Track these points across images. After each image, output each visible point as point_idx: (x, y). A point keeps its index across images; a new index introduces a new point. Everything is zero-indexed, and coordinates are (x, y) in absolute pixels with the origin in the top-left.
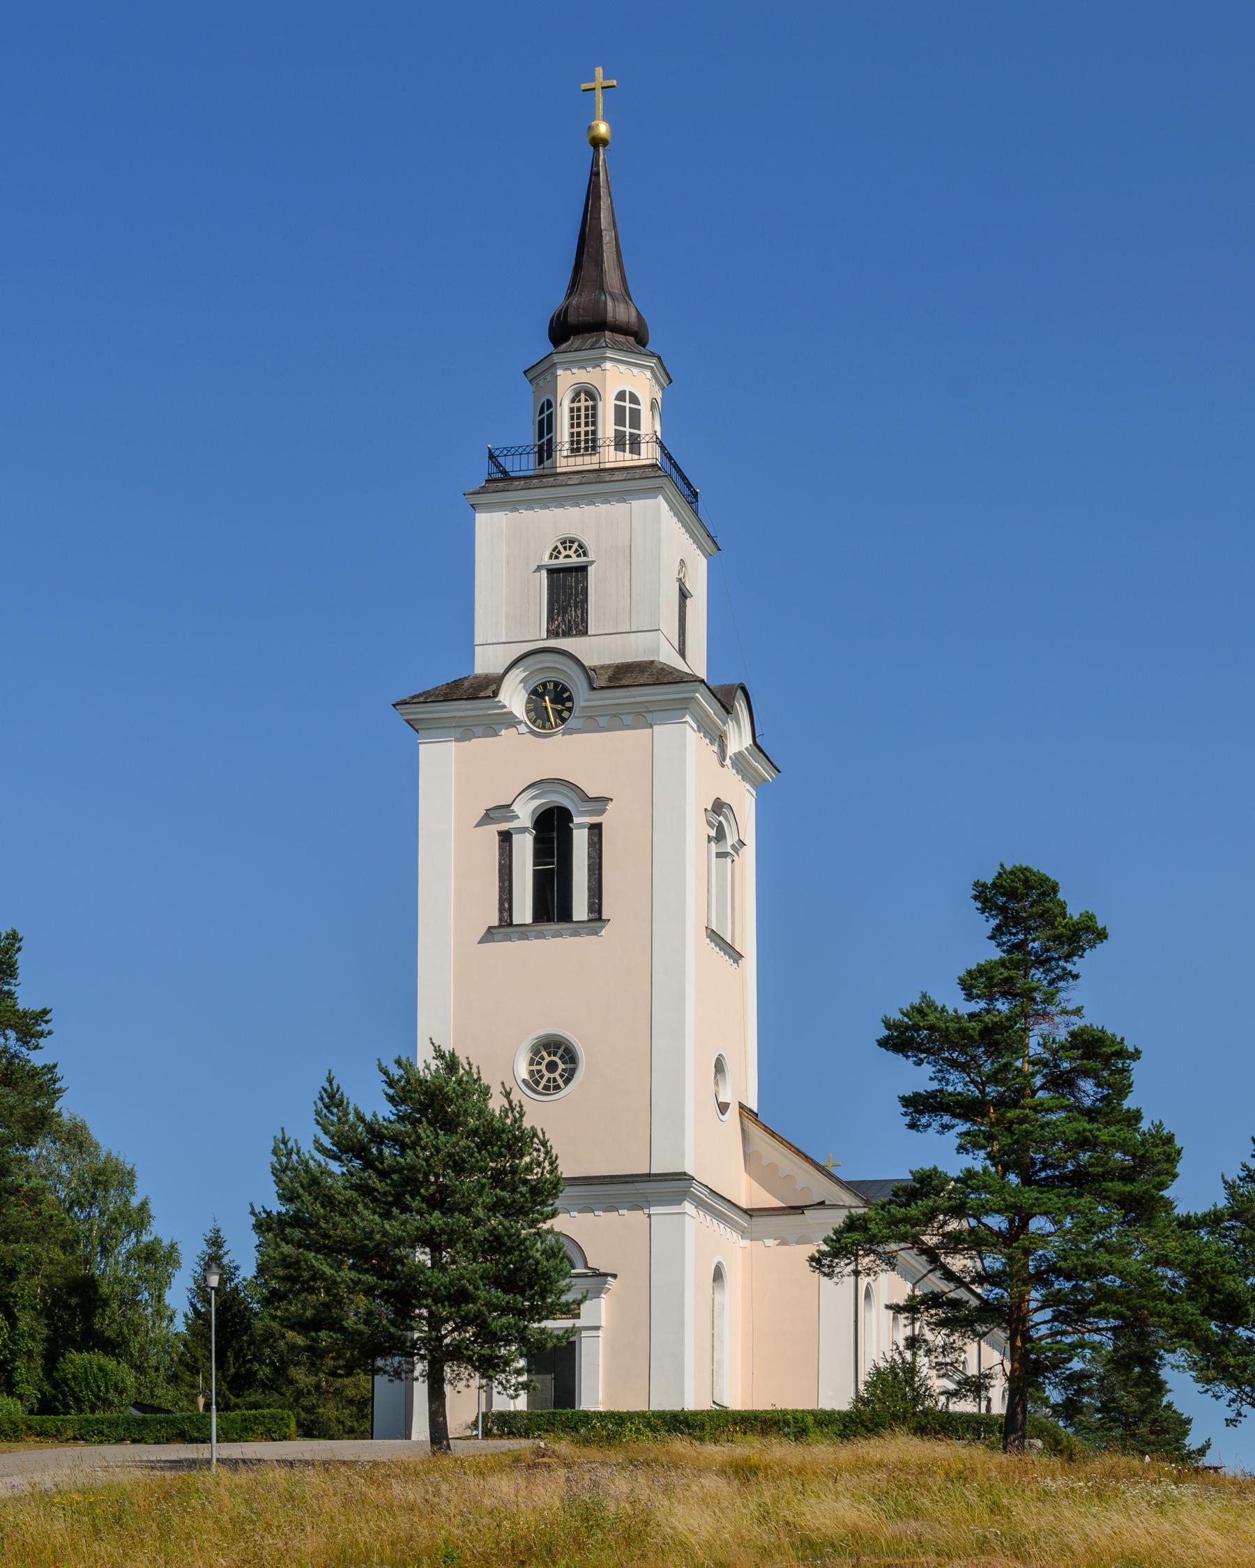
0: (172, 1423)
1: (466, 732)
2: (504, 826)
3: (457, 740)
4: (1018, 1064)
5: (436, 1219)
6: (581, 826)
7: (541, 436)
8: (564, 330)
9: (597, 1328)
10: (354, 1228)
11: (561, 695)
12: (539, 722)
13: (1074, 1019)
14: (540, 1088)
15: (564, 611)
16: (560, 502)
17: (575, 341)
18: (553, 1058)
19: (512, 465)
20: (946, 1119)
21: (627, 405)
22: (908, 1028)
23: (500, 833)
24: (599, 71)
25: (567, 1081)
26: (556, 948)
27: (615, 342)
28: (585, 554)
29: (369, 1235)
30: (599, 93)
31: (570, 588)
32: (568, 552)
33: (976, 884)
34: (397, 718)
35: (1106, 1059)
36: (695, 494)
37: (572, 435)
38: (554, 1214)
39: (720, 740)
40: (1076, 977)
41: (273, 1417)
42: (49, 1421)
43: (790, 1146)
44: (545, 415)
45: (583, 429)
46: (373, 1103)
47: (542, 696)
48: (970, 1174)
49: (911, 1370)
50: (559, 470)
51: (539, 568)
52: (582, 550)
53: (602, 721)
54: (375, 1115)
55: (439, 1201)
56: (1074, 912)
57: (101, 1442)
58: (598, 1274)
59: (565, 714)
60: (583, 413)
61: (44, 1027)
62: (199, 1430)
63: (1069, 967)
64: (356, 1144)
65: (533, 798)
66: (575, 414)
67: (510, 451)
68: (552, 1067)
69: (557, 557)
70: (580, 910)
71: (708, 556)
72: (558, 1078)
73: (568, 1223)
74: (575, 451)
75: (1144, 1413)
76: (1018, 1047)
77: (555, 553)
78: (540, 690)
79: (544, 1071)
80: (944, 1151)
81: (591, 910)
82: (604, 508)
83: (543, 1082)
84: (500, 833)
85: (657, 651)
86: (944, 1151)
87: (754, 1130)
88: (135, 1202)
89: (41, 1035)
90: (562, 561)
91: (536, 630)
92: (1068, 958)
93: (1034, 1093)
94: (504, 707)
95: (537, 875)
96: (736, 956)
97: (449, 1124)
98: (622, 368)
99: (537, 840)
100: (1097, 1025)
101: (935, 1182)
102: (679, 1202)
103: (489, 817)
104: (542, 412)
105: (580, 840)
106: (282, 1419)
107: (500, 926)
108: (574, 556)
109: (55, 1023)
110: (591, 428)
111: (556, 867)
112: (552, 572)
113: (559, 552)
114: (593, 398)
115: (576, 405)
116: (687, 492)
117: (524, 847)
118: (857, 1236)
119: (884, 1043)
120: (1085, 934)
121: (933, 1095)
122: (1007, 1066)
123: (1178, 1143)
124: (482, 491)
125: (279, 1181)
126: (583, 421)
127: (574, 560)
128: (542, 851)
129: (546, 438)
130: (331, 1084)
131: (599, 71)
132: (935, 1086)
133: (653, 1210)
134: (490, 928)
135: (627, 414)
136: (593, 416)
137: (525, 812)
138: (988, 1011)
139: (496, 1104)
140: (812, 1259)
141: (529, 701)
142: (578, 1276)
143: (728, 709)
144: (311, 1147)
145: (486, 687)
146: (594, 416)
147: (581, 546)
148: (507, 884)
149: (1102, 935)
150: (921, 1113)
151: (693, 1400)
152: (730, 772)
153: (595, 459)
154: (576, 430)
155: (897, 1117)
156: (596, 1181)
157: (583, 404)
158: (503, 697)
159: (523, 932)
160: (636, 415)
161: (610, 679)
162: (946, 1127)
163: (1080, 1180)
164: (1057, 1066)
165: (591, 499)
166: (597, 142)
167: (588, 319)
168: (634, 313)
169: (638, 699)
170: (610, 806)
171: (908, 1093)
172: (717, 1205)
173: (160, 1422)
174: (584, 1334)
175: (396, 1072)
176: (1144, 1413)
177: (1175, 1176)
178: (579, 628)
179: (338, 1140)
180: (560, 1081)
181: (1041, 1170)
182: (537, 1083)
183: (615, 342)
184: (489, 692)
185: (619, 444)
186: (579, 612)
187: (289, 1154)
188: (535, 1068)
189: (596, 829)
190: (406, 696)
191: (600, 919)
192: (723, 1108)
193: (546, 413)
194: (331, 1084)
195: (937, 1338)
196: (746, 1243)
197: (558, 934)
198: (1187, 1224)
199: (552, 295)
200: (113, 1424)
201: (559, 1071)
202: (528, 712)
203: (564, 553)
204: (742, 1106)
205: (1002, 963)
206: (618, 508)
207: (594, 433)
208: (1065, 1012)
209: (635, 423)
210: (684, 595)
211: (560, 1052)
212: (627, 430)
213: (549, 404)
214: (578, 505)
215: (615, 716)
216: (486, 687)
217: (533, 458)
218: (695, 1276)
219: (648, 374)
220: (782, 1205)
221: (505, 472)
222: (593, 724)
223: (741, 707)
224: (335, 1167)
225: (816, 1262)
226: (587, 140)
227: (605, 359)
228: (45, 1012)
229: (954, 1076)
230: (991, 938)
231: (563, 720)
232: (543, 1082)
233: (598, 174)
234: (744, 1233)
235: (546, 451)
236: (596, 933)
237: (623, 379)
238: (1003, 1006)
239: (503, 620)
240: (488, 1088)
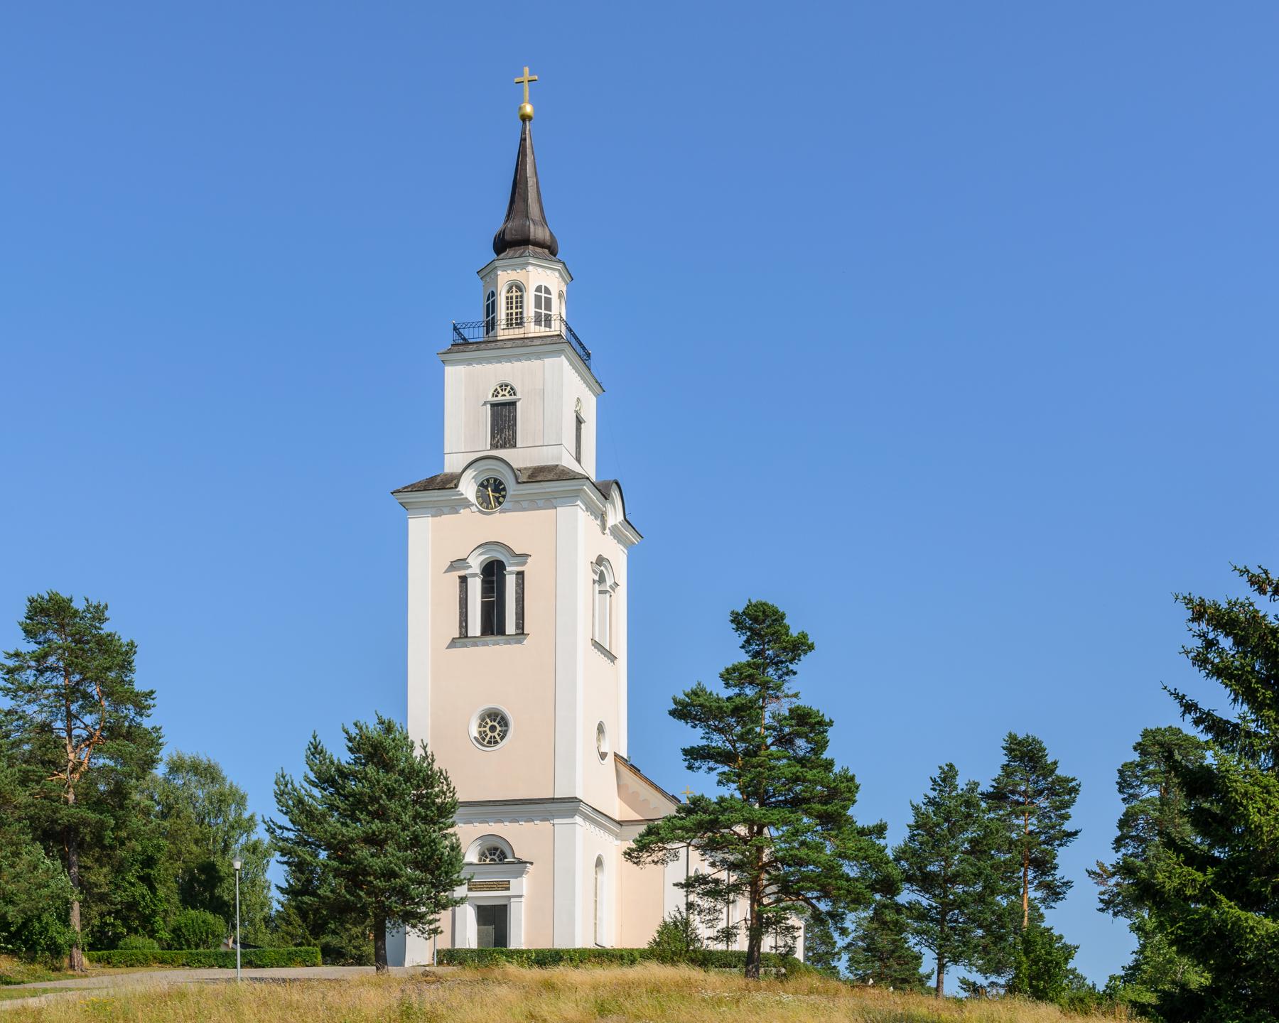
1: (438, 511)
2: (462, 573)
4: (758, 730)
5: (377, 825)
6: (511, 573)
8: (503, 245)
10: (326, 831)
11: (498, 487)
13: (794, 700)
15: (501, 431)
16: (499, 359)
17: (509, 252)
20: (712, 764)
21: (543, 295)
22: (688, 705)
23: (460, 577)
24: (526, 70)
25: (502, 738)
26: (495, 651)
27: (535, 252)
29: (334, 836)
30: (526, 84)
33: (732, 613)
34: (394, 501)
35: (812, 727)
36: (589, 355)
38: (452, 825)
39: (602, 517)
40: (795, 673)
41: (307, 952)
42: (168, 954)
45: (514, 311)
46: (341, 755)
47: (486, 487)
48: (722, 800)
49: (687, 923)
51: (485, 403)
53: (525, 504)
55: (381, 815)
56: (794, 633)
61: (150, 702)
63: (791, 667)
64: (330, 778)
67: (468, 325)
68: (493, 729)
70: (510, 628)
71: (597, 395)
74: (509, 324)
75: (893, 952)
76: (757, 720)
80: (708, 785)
81: (517, 627)
82: (526, 363)
84: (460, 577)
85: (560, 458)
86: (708, 785)
87: (625, 771)
88: (246, 815)
89: (149, 707)
90: (500, 399)
91: (483, 443)
92: (791, 661)
93: (768, 747)
96: (613, 658)
97: (387, 766)
98: (540, 270)
99: (484, 582)
100: (808, 704)
101: (703, 804)
102: (572, 816)
105: (511, 581)
109: (159, 701)
111: (495, 598)
112: (494, 405)
116: (582, 353)
117: (475, 586)
118: (652, 838)
119: (673, 713)
120: (799, 647)
121: (702, 748)
122: (750, 731)
123: (857, 781)
124: (449, 352)
125: (279, 801)
127: (508, 398)
131: (526, 70)
132: (704, 742)
133: (556, 821)
135: (543, 301)
137: (476, 564)
138: (739, 695)
139: (418, 753)
140: (625, 853)
141: (478, 491)
142: (509, 863)
143: (606, 496)
144: (302, 779)
145: (450, 482)
149: (811, 647)
150: (696, 759)
151: (582, 941)
152: (609, 538)
153: (522, 331)
155: (680, 762)
157: (514, 294)
158: (461, 488)
159: (475, 642)
160: (548, 301)
161: (529, 477)
162: (711, 769)
163: (796, 803)
164: (781, 730)
165: (518, 358)
166: (525, 118)
168: (548, 233)
170: (529, 560)
171: (687, 747)
172: (598, 817)
175: (354, 731)
176: (893, 952)
177: (855, 802)
178: (510, 442)
179: (319, 775)
181: (773, 796)
183: (535, 252)
185: (538, 321)
187: (286, 786)
189: (520, 575)
190: (399, 488)
192: (603, 756)
195: (705, 903)
196: (618, 842)
197: (497, 643)
198: (862, 832)
199: (495, 222)
200: (207, 956)
204: (616, 755)
205: (749, 665)
206: (535, 364)
208: (787, 696)
209: (548, 307)
210: (579, 421)
212: (543, 311)
213: (493, 294)
216: (450, 482)
217: (482, 331)
218: (583, 864)
219: (557, 274)
221: (464, 339)
222: (519, 506)
223: (615, 495)
224: (316, 792)
225: (628, 854)
227: (529, 264)
228: (152, 692)
229: (716, 736)
230: (743, 647)
231: (500, 503)
233: (525, 140)
234: (617, 836)
235: (491, 325)
237: (540, 277)
238: (750, 691)
239: (462, 438)
240: (413, 743)
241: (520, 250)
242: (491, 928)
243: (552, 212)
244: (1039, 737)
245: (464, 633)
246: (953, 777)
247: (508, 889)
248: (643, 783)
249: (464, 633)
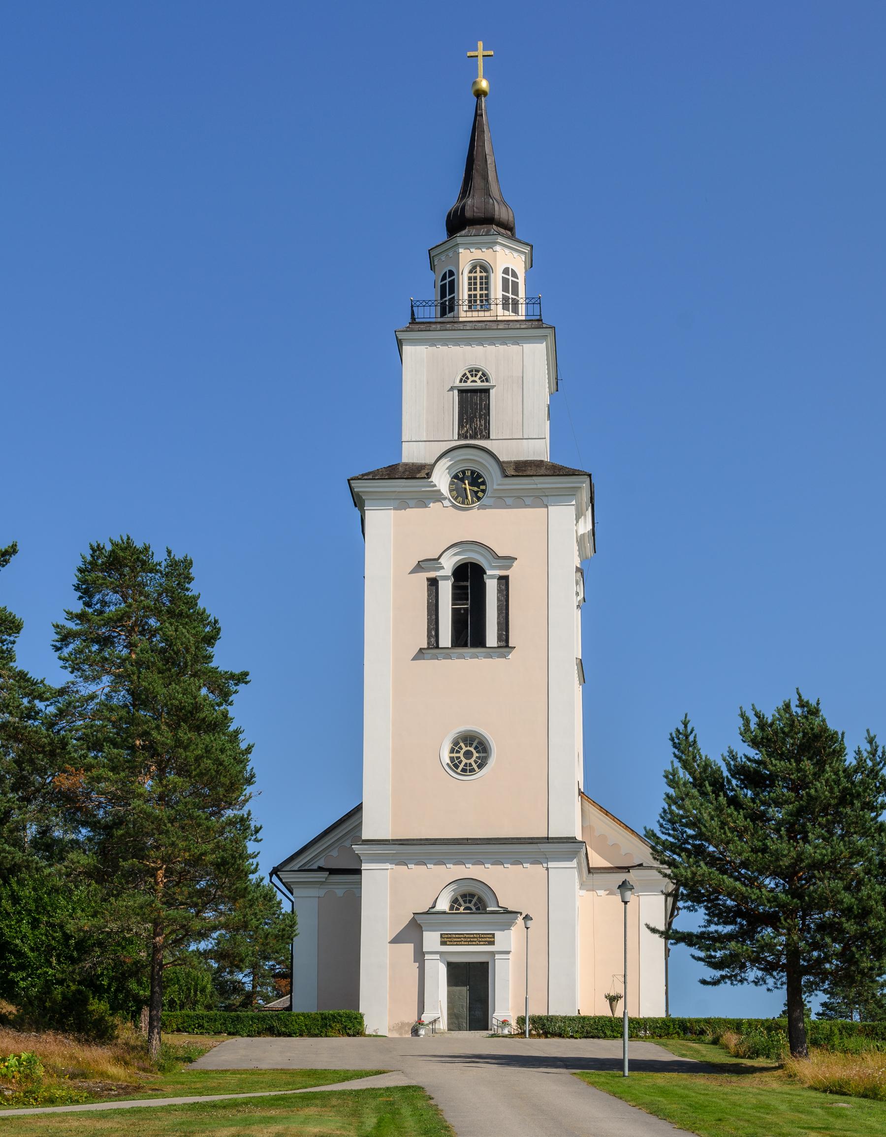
0: (263, 1019)
1: (402, 503)
2: (432, 574)
3: (395, 509)
6: (492, 577)
7: (443, 295)
8: (458, 223)
9: (508, 953)
11: (477, 480)
12: (460, 499)
14: (459, 770)
15: (471, 420)
16: (457, 342)
18: (469, 748)
19: (422, 314)
23: (428, 579)
24: (480, 44)
25: (480, 766)
26: (470, 666)
28: (487, 380)
30: (480, 61)
31: (476, 404)
32: (474, 378)
37: (470, 296)
43: (620, 822)
45: (478, 292)
47: (462, 480)
50: (461, 319)
51: (452, 389)
52: (485, 377)
57: (202, 1033)
58: (507, 912)
59: (480, 494)
60: (478, 281)
62: (286, 1026)
65: (455, 555)
66: (472, 282)
69: (465, 382)
70: (492, 639)
72: (473, 764)
77: (464, 379)
78: (461, 476)
79: (462, 758)
81: (499, 639)
82: (502, 348)
83: (461, 766)
84: (428, 579)
90: (469, 384)
94: (435, 486)
95: (455, 611)
98: (507, 251)
99: (454, 587)
103: (420, 567)
104: (444, 278)
105: (492, 587)
106: (356, 1018)
107: (428, 648)
108: (479, 381)
110: (484, 292)
111: (470, 608)
112: (461, 392)
113: (467, 378)
114: (486, 271)
115: (473, 275)
117: (446, 589)
126: (478, 286)
127: (479, 384)
128: (458, 594)
129: (448, 298)
130: (686, 726)
131: (480, 44)
133: (551, 865)
134: (421, 649)
136: (486, 283)
137: (449, 564)
141: (452, 483)
146: (487, 283)
147: (484, 374)
148: (434, 617)
154: (473, 293)
156: (510, 841)
157: (478, 275)
165: (481, 342)
166: (479, 94)
167: (482, 215)
168: (511, 215)
169: (539, 486)
170: (516, 563)
173: (252, 1018)
174: (497, 956)
180: (475, 766)
182: (457, 766)
184: (423, 474)
186: (483, 422)
188: (455, 755)
189: (504, 581)
191: (507, 646)
193: (448, 280)
194: (686, 726)
201: (474, 758)
202: (451, 491)
203: (471, 379)
206: (512, 349)
207: (487, 295)
209: (515, 292)
212: (510, 296)
214: (483, 345)
215: (519, 497)
216: (418, 472)
220: (610, 865)
222: (501, 502)
226: (472, 92)
232: (461, 766)
235: (448, 307)
236: (505, 657)
237: (506, 259)
239: (425, 427)
241: (483, 229)
242: (464, 990)
243: (505, 190)
247: (492, 943)
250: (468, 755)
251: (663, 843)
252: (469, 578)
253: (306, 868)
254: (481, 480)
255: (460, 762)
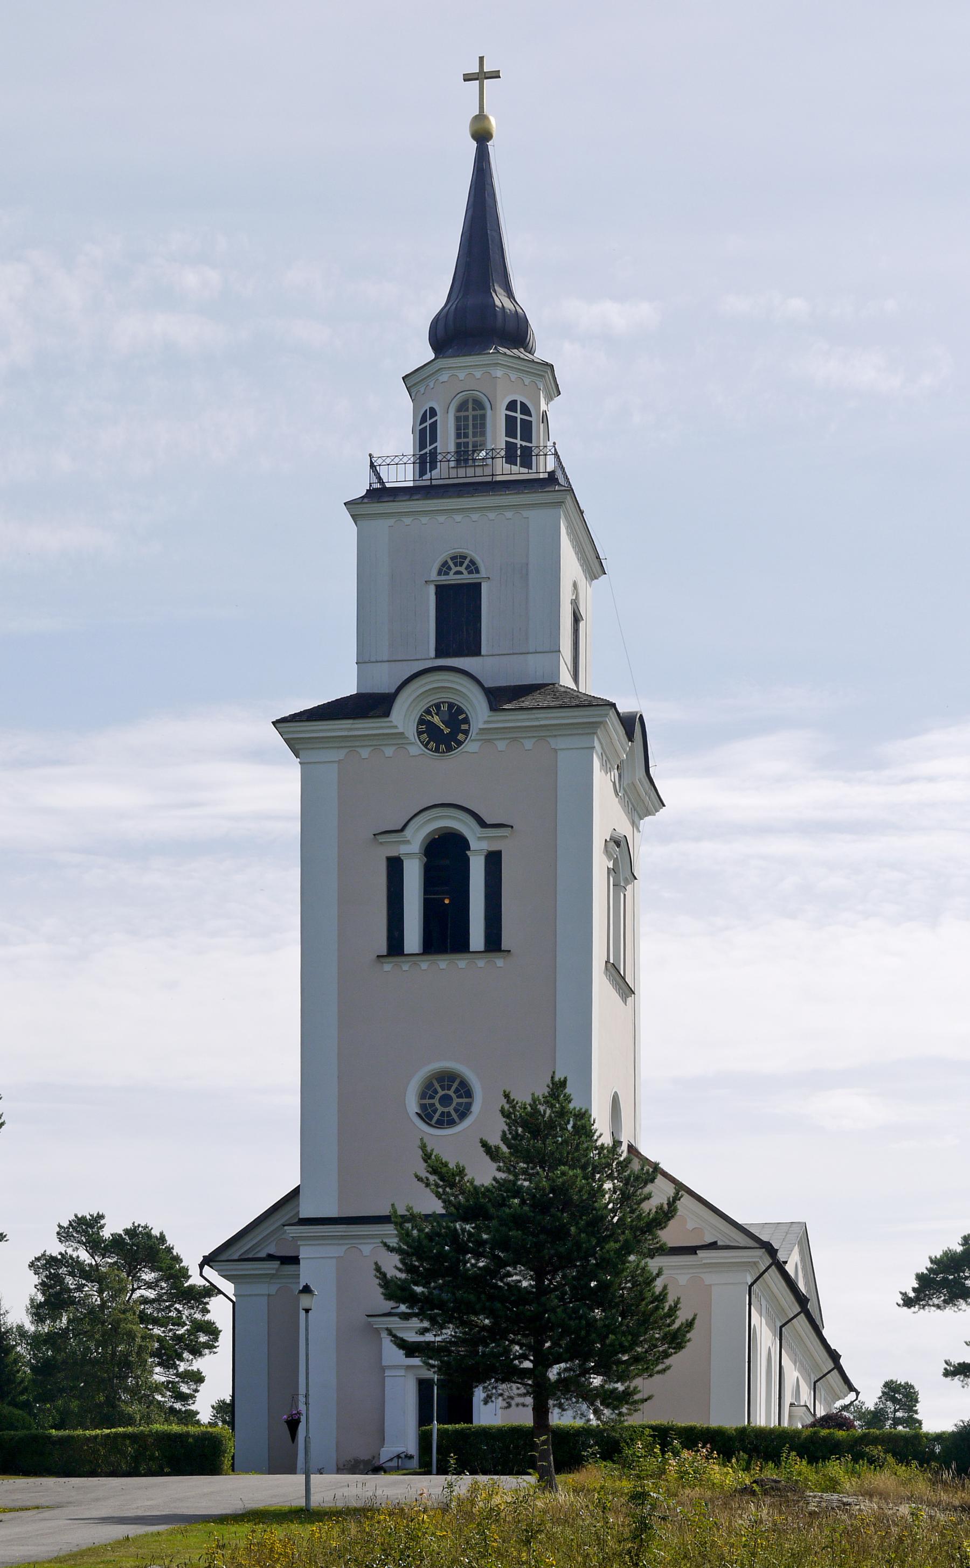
21: (519, 416)
28: (478, 571)
32: (459, 568)
44: (427, 424)
52: (473, 567)
54: (432, 1150)
70: (477, 938)
73: (673, 1277)
77: (444, 569)
79: (438, 1105)
104: (423, 420)
108: (465, 572)
113: (450, 569)
115: (462, 414)
127: (466, 578)
136: (480, 424)
171: (910, 1285)
182: (430, 1117)
185: (511, 455)
189: (494, 860)
193: (429, 422)
202: (420, 733)
211: (455, 1085)
212: (519, 442)
244: (920, 1397)
245: (395, 946)
246: (53, 1259)
248: (822, 1348)
249: (395, 946)
250: (446, 1100)
251: (158, 1299)
252: (446, 855)
253: (250, 1256)
254: (464, 716)
255: (435, 1111)
